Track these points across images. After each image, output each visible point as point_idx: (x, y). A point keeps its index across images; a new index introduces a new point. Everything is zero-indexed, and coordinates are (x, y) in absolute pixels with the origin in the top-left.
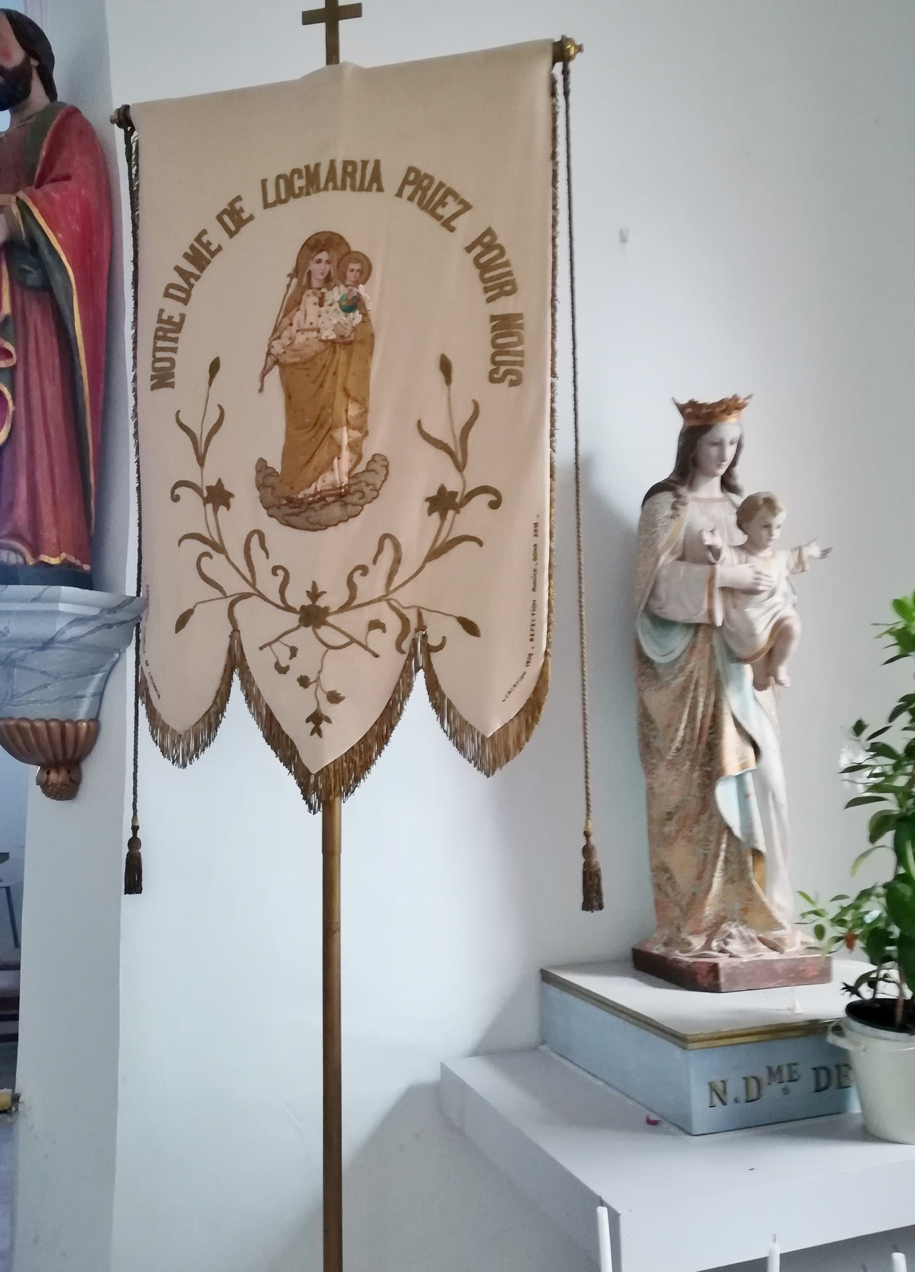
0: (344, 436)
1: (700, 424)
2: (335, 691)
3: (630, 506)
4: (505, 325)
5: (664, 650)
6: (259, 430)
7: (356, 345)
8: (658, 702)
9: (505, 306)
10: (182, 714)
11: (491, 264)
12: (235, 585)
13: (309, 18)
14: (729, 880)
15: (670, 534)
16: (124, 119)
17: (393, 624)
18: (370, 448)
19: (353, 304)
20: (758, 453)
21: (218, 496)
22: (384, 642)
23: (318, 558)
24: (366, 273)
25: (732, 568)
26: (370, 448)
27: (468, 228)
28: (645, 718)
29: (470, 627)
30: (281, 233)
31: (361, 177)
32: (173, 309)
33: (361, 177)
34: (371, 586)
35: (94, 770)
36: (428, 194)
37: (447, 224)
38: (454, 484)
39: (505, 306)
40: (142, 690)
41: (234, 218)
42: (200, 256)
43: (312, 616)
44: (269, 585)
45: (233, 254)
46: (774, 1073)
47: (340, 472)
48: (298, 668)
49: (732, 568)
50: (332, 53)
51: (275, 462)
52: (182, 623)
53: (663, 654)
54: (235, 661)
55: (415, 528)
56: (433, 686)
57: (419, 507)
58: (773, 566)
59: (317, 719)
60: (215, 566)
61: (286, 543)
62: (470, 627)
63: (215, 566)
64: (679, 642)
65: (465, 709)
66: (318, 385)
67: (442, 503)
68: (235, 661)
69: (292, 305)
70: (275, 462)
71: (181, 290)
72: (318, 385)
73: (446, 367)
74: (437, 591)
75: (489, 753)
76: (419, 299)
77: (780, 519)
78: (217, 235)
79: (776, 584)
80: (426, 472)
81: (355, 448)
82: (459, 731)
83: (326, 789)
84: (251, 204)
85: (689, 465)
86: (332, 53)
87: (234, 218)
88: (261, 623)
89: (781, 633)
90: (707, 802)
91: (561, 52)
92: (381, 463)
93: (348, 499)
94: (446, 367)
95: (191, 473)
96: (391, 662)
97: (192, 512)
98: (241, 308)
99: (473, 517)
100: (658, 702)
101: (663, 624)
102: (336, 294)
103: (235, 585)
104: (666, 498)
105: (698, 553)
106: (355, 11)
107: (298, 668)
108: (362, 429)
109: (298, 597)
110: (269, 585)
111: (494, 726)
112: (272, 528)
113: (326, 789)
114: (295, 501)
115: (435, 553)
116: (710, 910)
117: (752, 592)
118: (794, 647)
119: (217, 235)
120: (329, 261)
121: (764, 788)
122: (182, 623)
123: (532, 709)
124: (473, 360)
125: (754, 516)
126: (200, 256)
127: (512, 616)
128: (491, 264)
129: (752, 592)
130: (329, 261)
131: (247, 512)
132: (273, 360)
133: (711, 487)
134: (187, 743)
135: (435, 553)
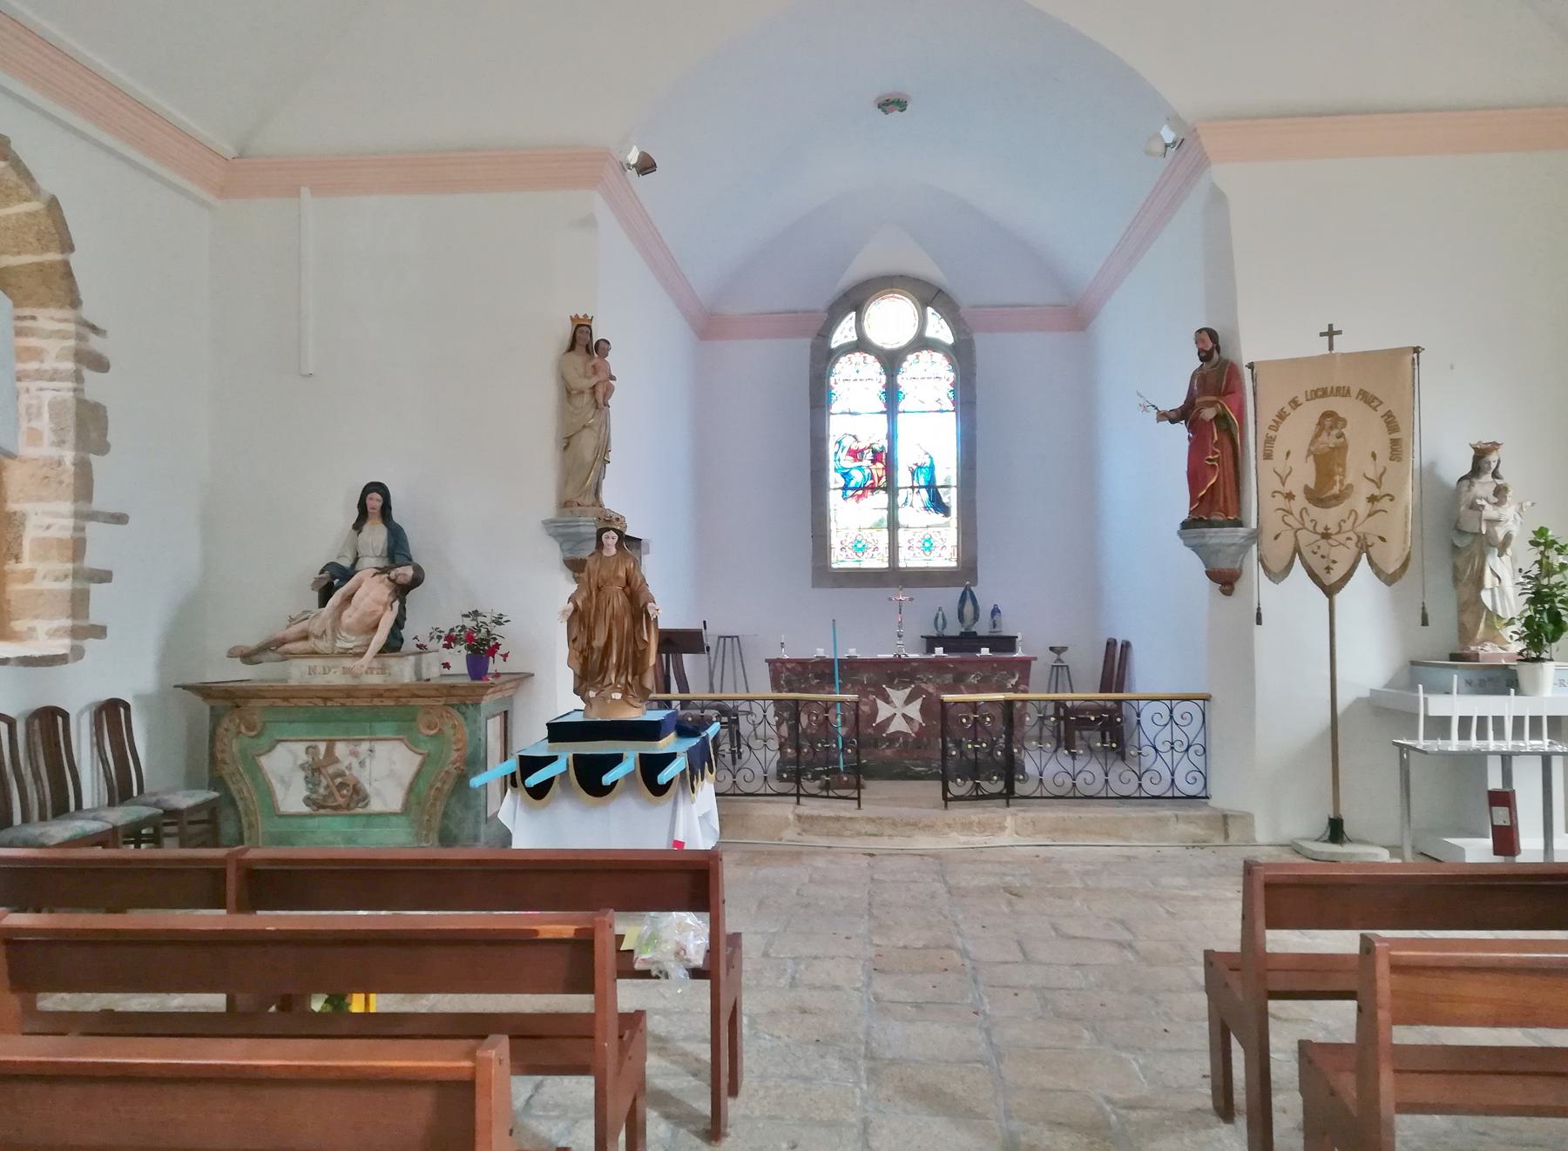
0: (1337, 478)
1: (1481, 456)
2: (104, 408)
3: (1453, 482)
4: (1395, 443)
5: (1462, 542)
6: (1304, 474)
7: (1342, 449)
8: (1460, 562)
9: (1395, 436)
10: (1276, 567)
11: (1390, 422)
12: (1297, 525)
13: (1322, 334)
14: (1487, 626)
15: (1466, 498)
16: (1251, 366)
17: (1355, 538)
18: (1348, 481)
19: (1341, 435)
20: (1508, 462)
21: (1290, 496)
22: (1351, 544)
23: (1329, 517)
24: (1344, 426)
25: (1490, 512)
26: (1348, 481)
27: (1382, 410)
28: (1455, 568)
29: (1383, 539)
30: (1311, 413)
31: (1343, 392)
32: (1272, 433)
33: (1343, 392)
34: (1347, 526)
35: (1239, 586)
36: (1367, 398)
37: (1375, 409)
38: (1377, 492)
39: (1395, 436)
40: (1260, 560)
41: (1295, 403)
42: (1282, 416)
43: (1326, 536)
44: (1310, 525)
45: (1294, 416)
46: (1490, 679)
47: (1336, 490)
48: (1320, 552)
49: (1490, 512)
50: (1331, 348)
51: (1312, 486)
52: (1276, 537)
53: (1462, 543)
54: (1297, 550)
55: (1363, 507)
56: (1369, 558)
57: (1363, 501)
58: (1509, 512)
59: (1328, 569)
60: (1289, 519)
61: (1315, 512)
62: (1383, 539)
63: (1289, 519)
64: (1467, 541)
65: (1381, 565)
66: (1328, 463)
67: (1372, 499)
68: (1297, 550)
69: (1317, 436)
70: (1312, 486)
71: (1275, 427)
72: (1328, 463)
73: (1374, 455)
74: (1370, 527)
75: (1390, 579)
76: (1363, 434)
77: (1510, 494)
78: (1288, 409)
79: (1512, 520)
80: (1367, 489)
81: (1341, 482)
82: (1379, 573)
83: (1330, 591)
84: (1301, 399)
85: (1477, 469)
86: (1331, 348)
87: (1295, 403)
88: (1305, 538)
89: (1508, 537)
90: (1479, 600)
91: (1416, 350)
92: (1350, 486)
93: (1338, 499)
94: (1374, 455)
95: (1279, 487)
96: (1354, 550)
97: (1280, 501)
98: (1298, 434)
99: (1384, 504)
100: (1460, 562)
101: (1461, 532)
102: (1335, 432)
103: (1297, 525)
104: (1466, 482)
105: (1474, 507)
106: (1339, 332)
107: (1320, 552)
108: (1343, 475)
109: (1320, 529)
110: (1310, 525)
111: (1391, 571)
112: (1310, 507)
113: (1330, 591)
114: (1318, 497)
115: (1369, 515)
116: (1479, 637)
117: (1498, 521)
118: (1513, 542)
119: (1288, 409)
120: (1330, 420)
121: (1502, 592)
122: (1276, 537)
123: (1405, 566)
124: (1384, 452)
125: (1500, 492)
126: (1282, 416)
127: (1399, 529)
128: (1390, 422)
129: (1498, 521)
130: (1330, 420)
131: (1300, 501)
132: (1310, 453)
133: (1488, 477)
134: (1278, 575)
135: (1369, 515)
